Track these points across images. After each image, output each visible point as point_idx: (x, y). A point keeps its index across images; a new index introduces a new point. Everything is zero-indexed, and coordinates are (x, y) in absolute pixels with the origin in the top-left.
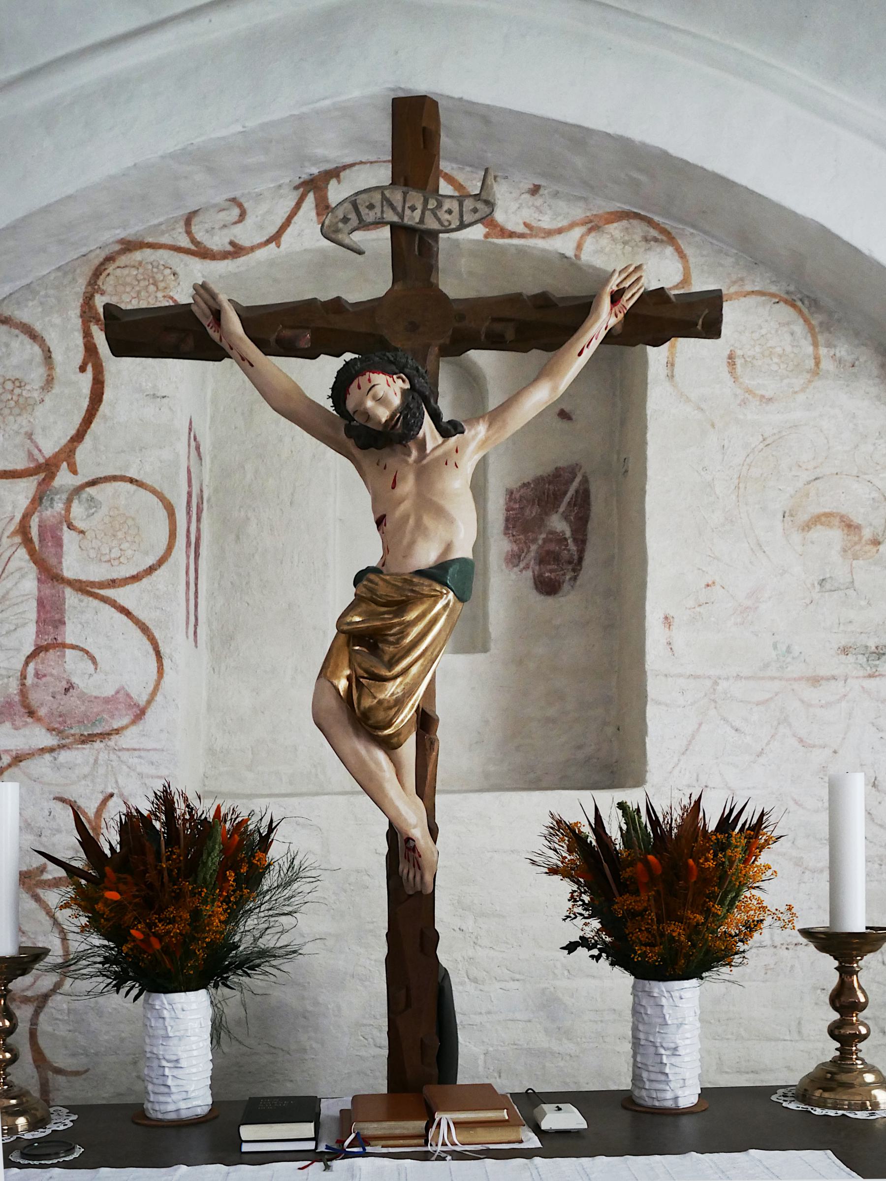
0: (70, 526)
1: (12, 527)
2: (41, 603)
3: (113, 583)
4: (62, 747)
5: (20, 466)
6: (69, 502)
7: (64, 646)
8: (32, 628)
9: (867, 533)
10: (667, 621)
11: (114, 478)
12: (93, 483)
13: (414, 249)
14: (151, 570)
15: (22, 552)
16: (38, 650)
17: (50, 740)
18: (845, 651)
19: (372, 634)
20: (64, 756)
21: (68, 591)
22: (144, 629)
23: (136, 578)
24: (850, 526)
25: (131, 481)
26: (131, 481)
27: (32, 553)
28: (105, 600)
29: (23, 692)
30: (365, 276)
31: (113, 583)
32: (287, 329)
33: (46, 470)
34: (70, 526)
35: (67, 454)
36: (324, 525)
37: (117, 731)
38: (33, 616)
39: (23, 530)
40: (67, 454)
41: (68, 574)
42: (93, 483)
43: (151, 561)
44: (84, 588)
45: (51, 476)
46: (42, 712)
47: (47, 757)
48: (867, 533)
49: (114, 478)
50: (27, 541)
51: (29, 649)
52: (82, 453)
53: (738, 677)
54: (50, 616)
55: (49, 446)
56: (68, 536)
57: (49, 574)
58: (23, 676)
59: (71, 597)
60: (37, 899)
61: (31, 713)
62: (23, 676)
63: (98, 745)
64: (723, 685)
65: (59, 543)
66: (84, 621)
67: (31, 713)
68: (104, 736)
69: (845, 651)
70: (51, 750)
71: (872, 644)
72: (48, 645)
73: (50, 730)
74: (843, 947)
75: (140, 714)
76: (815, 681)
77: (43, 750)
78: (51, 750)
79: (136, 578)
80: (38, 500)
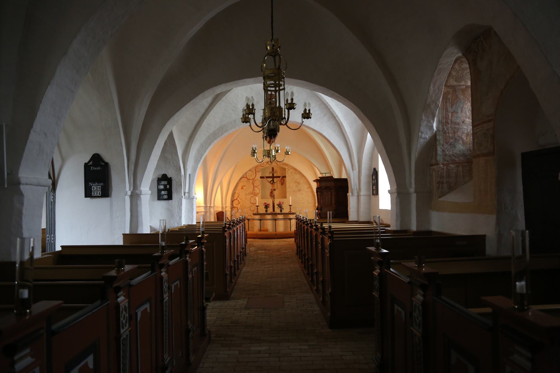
13: (273, 174)
19: (272, 192)
30: (271, 175)
32: (267, 177)
36: (269, 186)
54: (254, 188)
66: (256, 189)
74: (290, 206)
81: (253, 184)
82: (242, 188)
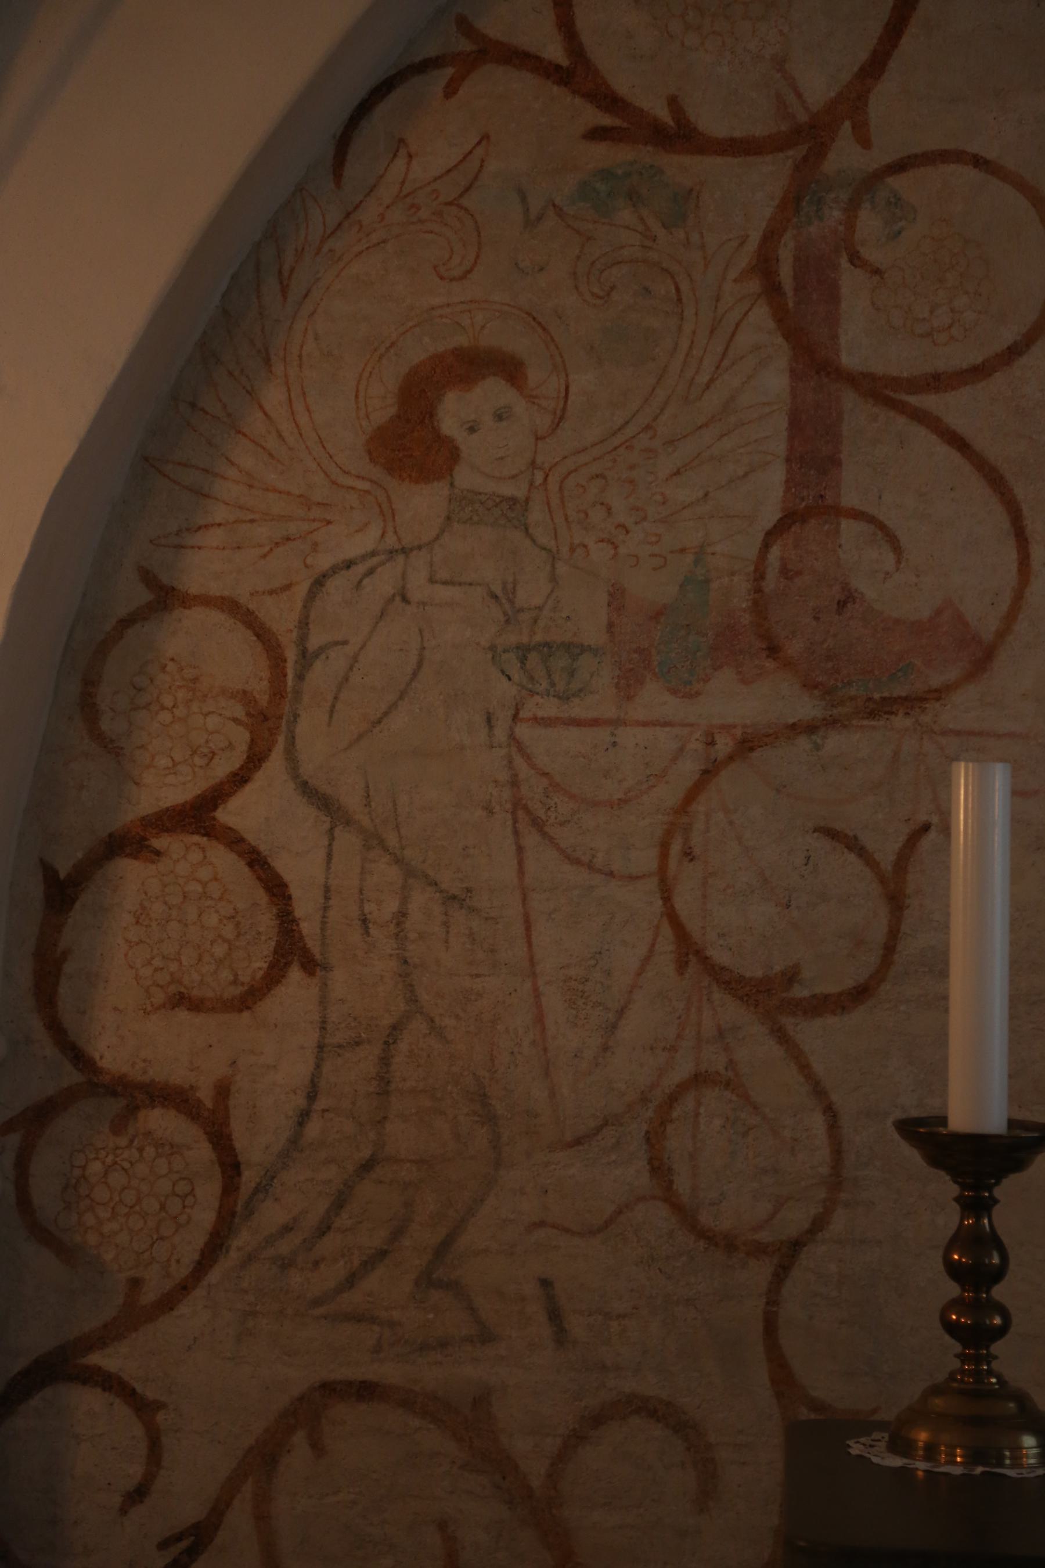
0: (855, 259)
1: (745, 258)
2: (795, 423)
3: (937, 382)
4: (832, 723)
5: (759, 131)
6: (853, 207)
7: (838, 511)
8: (776, 475)
11: (944, 156)
12: (900, 167)
14: (1013, 352)
15: (761, 314)
16: (789, 520)
17: (807, 708)
20: (834, 742)
21: (849, 399)
22: (995, 480)
23: (979, 372)
25: (978, 162)
26: (978, 162)
27: (781, 316)
28: (920, 416)
29: (759, 606)
31: (937, 382)
33: (807, 137)
34: (855, 259)
35: (852, 103)
37: (938, 694)
38: (779, 446)
39: (764, 266)
40: (852, 103)
41: (848, 360)
42: (900, 167)
43: (1009, 335)
44: (880, 390)
45: (820, 151)
46: (794, 648)
47: (803, 743)
49: (944, 156)
50: (772, 290)
51: (770, 516)
52: (883, 101)
54: (813, 451)
55: (818, 86)
56: (850, 281)
57: (813, 360)
58: (759, 575)
59: (857, 414)
60: (782, 1037)
61: (773, 650)
62: (759, 575)
63: (900, 721)
65: (833, 297)
66: (887, 466)
67: (773, 650)
68: (912, 702)
70: (811, 728)
72: (809, 508)
73: (809, 685)
75: (982, 657)
77: (795, 729)
78: (811, 728)
79: (979, 372)
80: (793, 203)
81: (797, 297)
82: (411, 445)
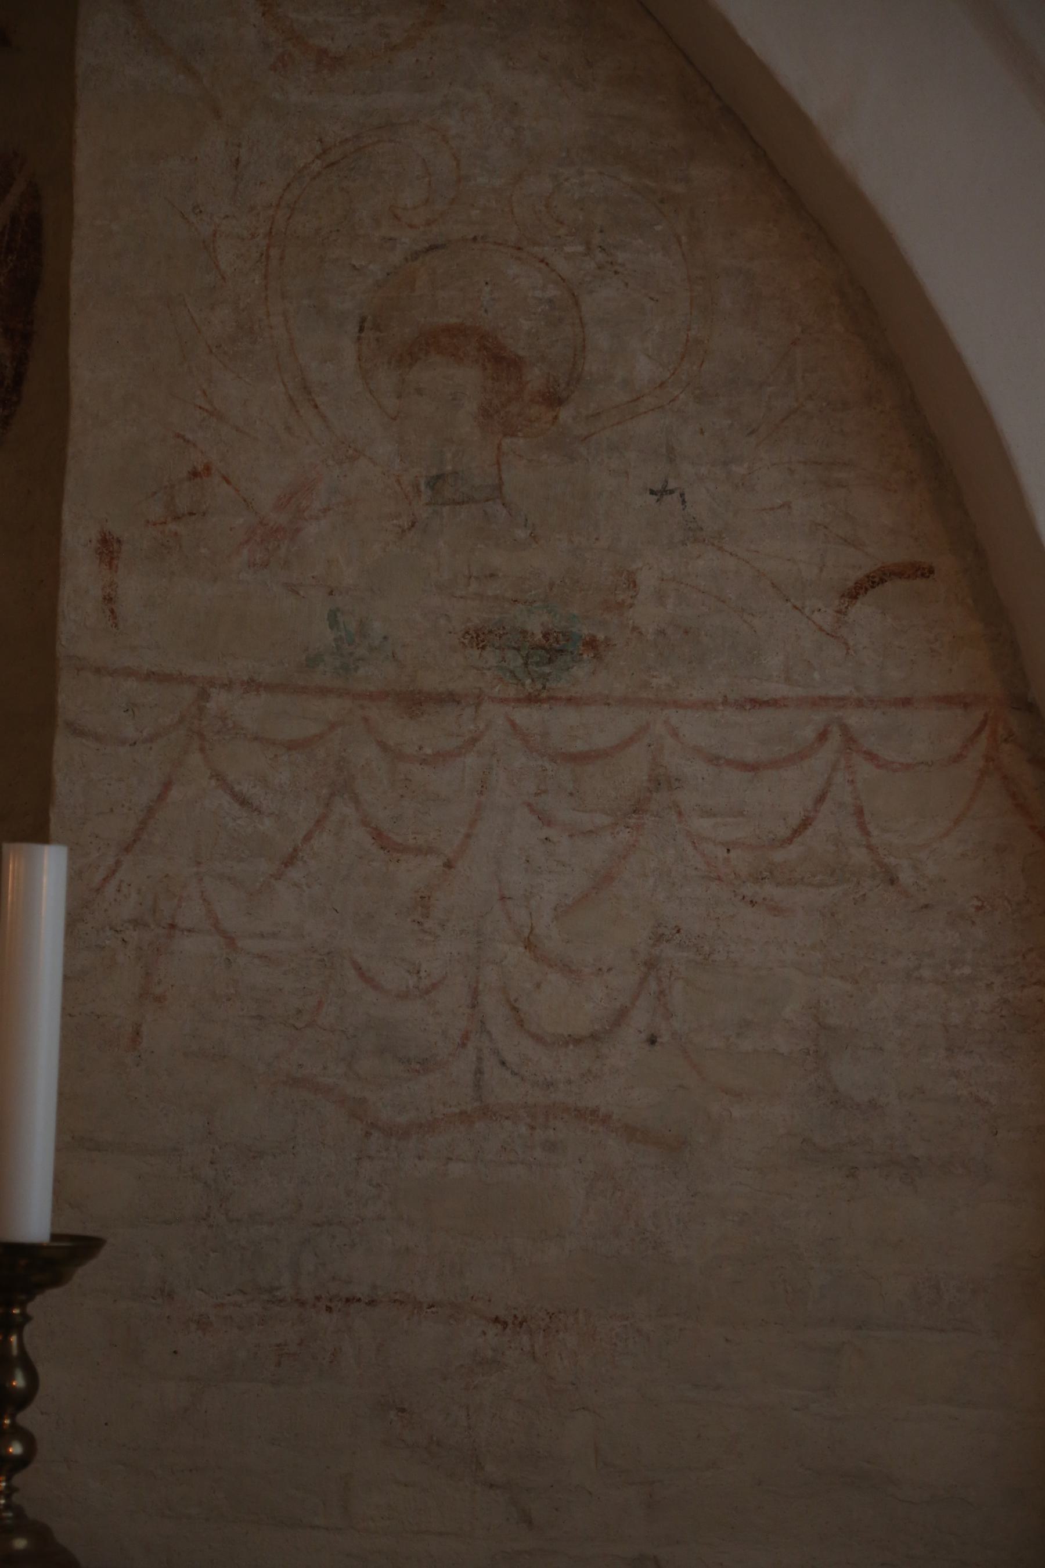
9: (535, 377)
10: (108, 548)
18: (478, 638)
24: (501, 362)
48: (535, 377)
53: (252, 685)
64: (219, 699)
69: (478, 638)
71: (535, 625)
76: (414, 702)
